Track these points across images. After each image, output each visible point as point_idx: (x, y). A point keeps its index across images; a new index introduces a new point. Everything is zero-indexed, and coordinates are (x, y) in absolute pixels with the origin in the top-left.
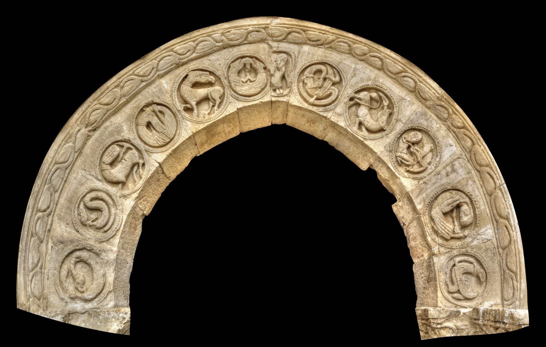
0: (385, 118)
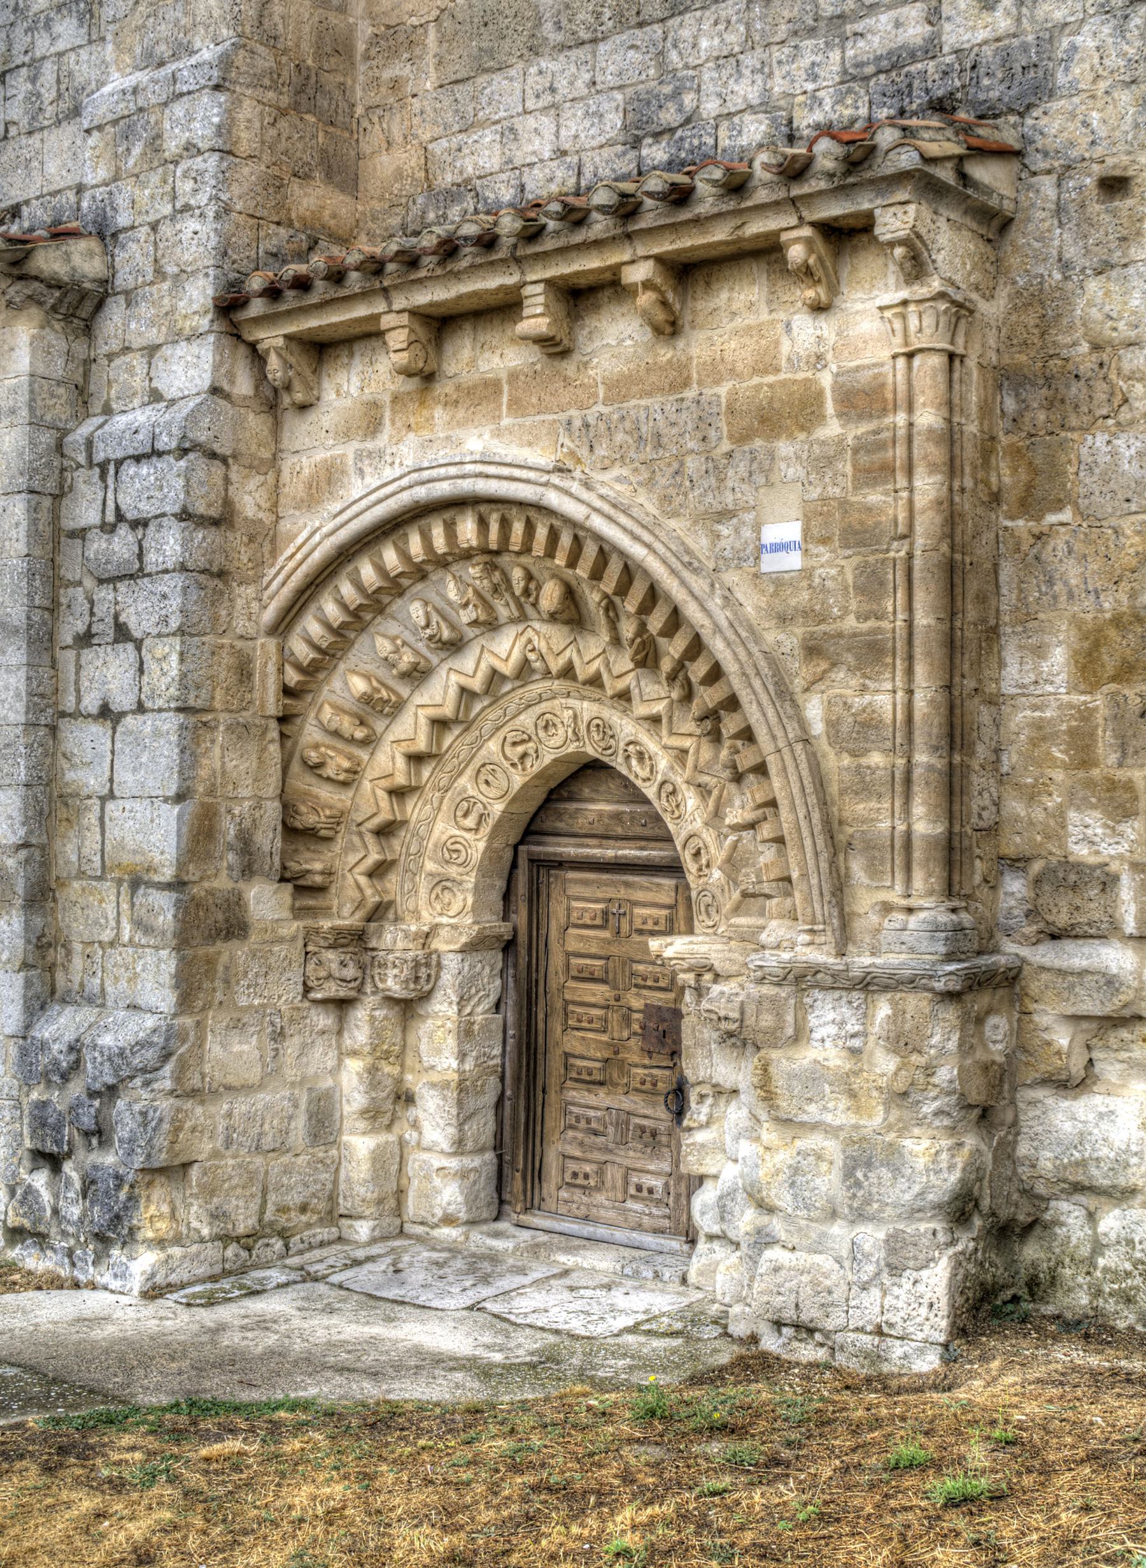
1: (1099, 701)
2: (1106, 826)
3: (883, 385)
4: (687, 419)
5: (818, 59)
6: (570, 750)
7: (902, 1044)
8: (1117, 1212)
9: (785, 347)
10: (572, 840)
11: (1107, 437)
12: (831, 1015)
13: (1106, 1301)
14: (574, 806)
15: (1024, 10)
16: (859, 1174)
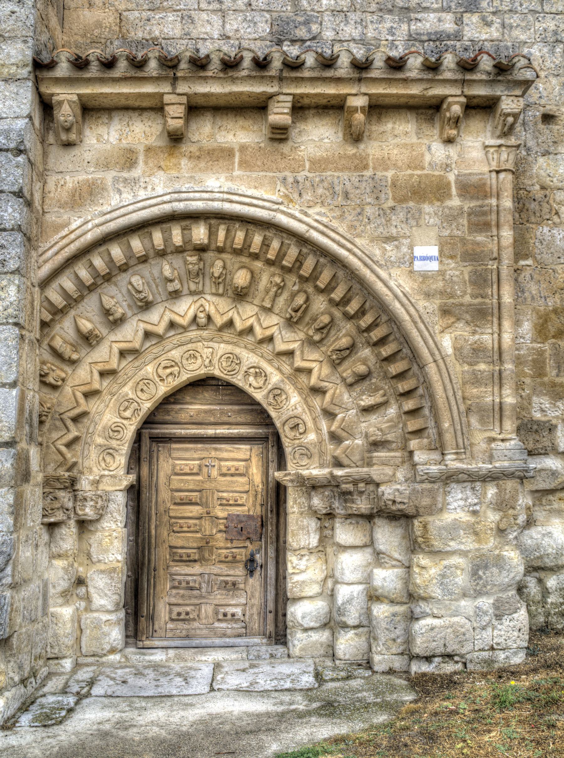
0: (262, 382)
1: (547, 347)
2: (551, 403)
3: (484, 184)
4: (366, 187)
5: (395, 26)
6: (202, 372)
7: (504, 505)
8: (555, 577)
9: (427, 158)
10: (176, 426)
11: (549, 228)
12: (460, 496)
13: (552, 617)
14: (179, 407)
15: (506, 31)
16: (481, 573)
